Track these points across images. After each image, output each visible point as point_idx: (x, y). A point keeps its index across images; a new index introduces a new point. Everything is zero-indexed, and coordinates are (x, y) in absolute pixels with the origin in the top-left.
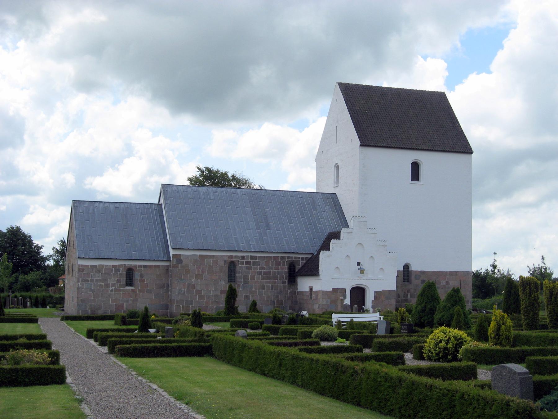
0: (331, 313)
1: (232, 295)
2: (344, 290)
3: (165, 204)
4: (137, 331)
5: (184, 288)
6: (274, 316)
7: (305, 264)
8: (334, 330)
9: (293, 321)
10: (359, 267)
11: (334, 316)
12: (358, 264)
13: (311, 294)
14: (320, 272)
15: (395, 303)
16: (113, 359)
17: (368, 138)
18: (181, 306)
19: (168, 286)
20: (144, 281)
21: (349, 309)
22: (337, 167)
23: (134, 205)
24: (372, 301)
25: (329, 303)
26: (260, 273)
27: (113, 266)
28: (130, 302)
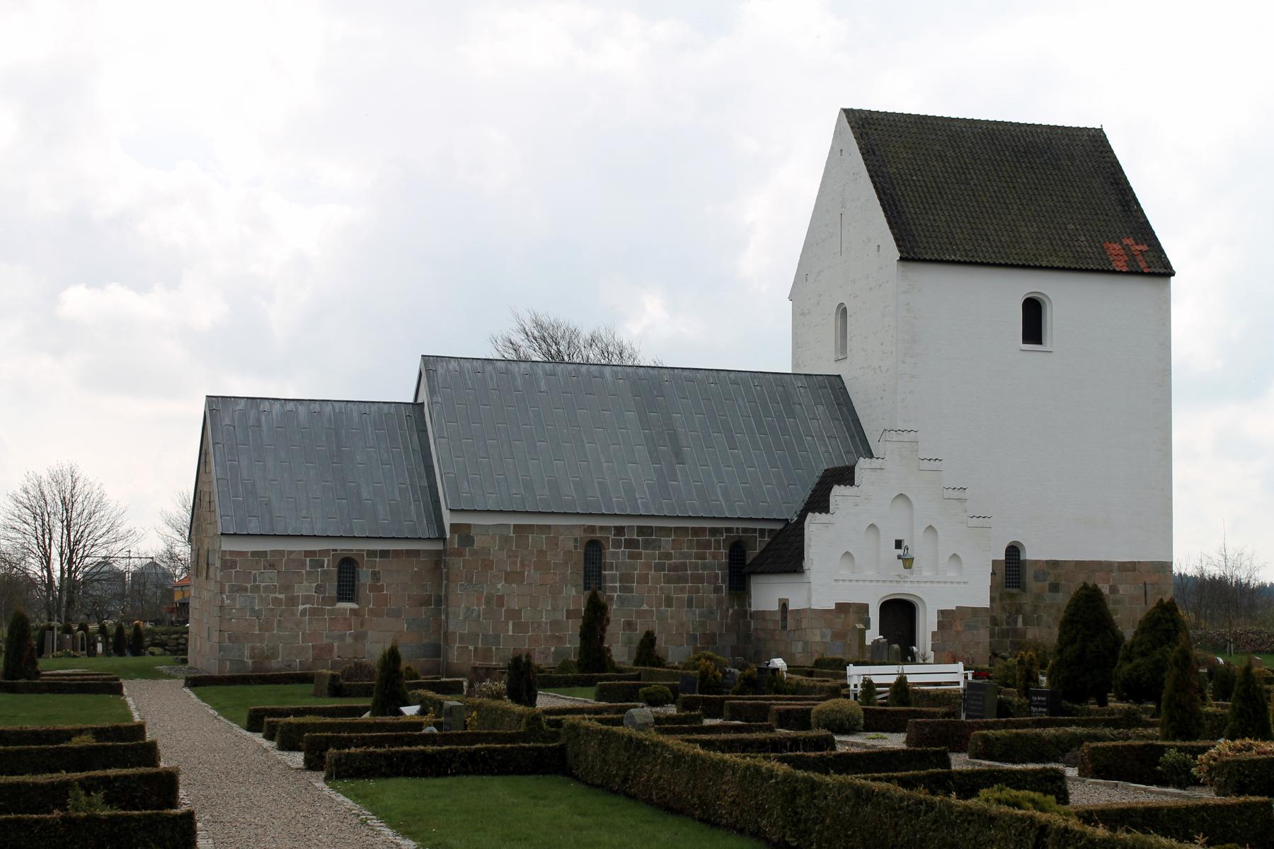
0: (841, 665)
1: (595, 618)
2: (864, 608)
3: (431, 403)
4: (367, 715)
5: (478, 605)
6: (702, 672)
7: (769, 544)
8: (852, 706)
9: (751, 684)
10: (900, 552)
11: (852, 670)
12: (898, 544)
13: (784, 618)
14: (806, 564)
15: (988, 640)
16: (318, 780)
17: (918, 243)
18: (471, 648)
19: (439, 601)
20: (381, 589)
21: (876, 656)
22: (843, 312)
23: (354, 407)
24: (933, 633)
25: (828, 639)
26: (660, 567)
27: (308, 553)
28: (349, 640)
